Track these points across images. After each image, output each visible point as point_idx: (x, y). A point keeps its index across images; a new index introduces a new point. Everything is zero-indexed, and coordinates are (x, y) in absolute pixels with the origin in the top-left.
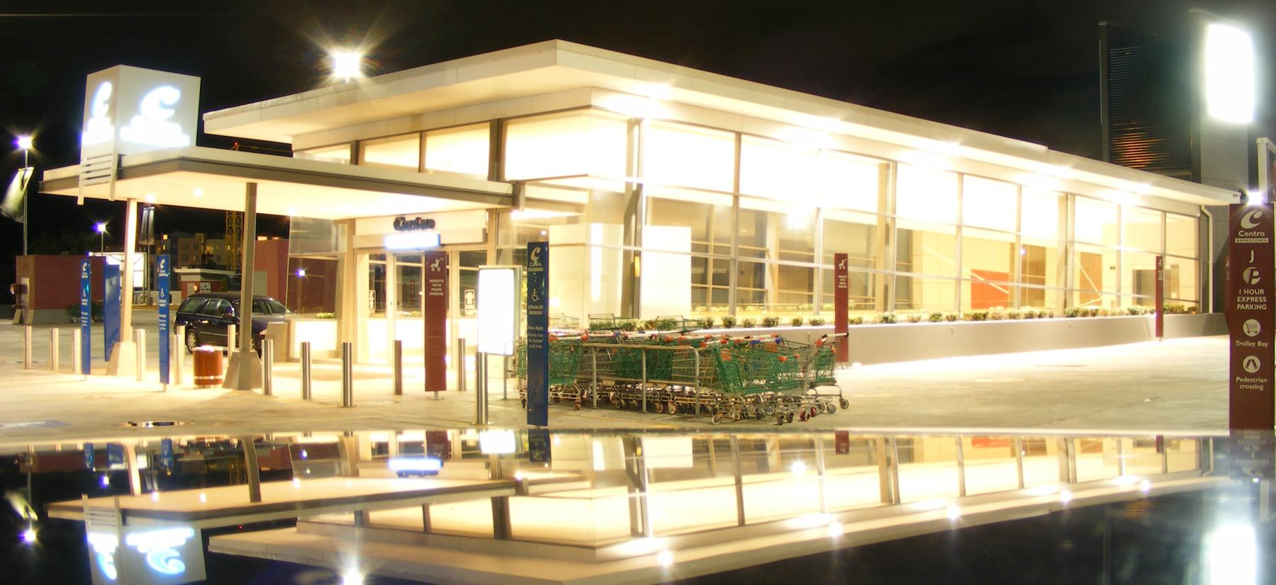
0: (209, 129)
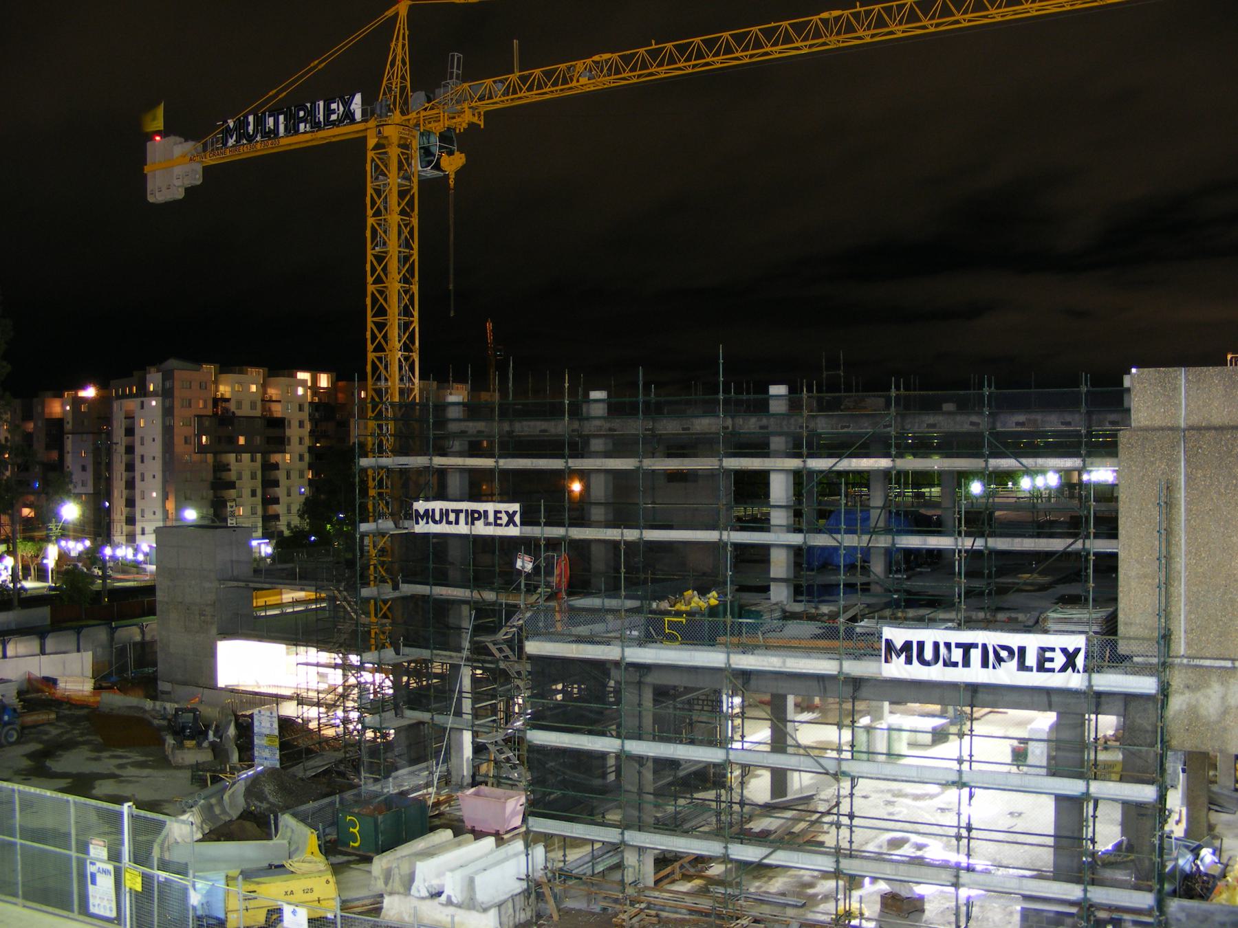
0: (973, 651)
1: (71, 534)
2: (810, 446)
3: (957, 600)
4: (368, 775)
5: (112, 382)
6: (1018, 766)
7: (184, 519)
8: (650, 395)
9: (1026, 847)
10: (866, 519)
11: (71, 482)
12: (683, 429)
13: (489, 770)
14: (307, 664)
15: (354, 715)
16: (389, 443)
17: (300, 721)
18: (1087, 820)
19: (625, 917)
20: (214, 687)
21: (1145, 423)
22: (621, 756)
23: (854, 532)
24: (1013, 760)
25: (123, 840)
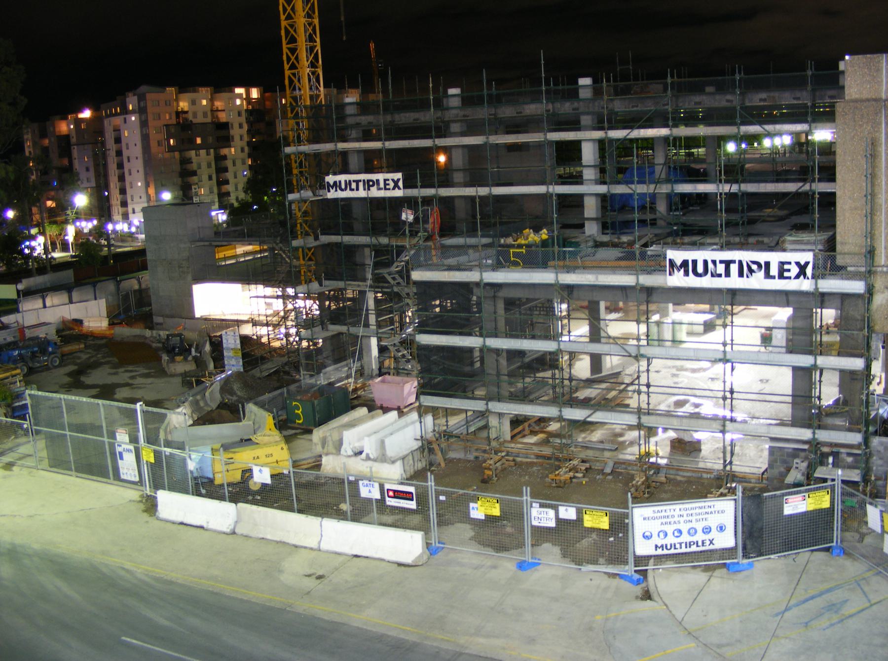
0: (732, 266)
1: (83, 217)
2: (609, 121)
3: (719, 229)
4: (305, 373)
5: (102, 106)
6: (765, 347)
7: (162, 200)
8: (492, 90)
9: (772, 404)
10: (652, 173)
11: (79, 179)
12: (517, 113)
13: (390, 364)
14: (257, 297)
15: (293, 331)
16: (304, 135)
17: (255, 337)
18: (815, 384)
19: (492, 462)
20: (193, 318)
21: (855, 96)
22: (484, 350)
23: (643, 182)
24: (762, 343)
25: (138, 428)
